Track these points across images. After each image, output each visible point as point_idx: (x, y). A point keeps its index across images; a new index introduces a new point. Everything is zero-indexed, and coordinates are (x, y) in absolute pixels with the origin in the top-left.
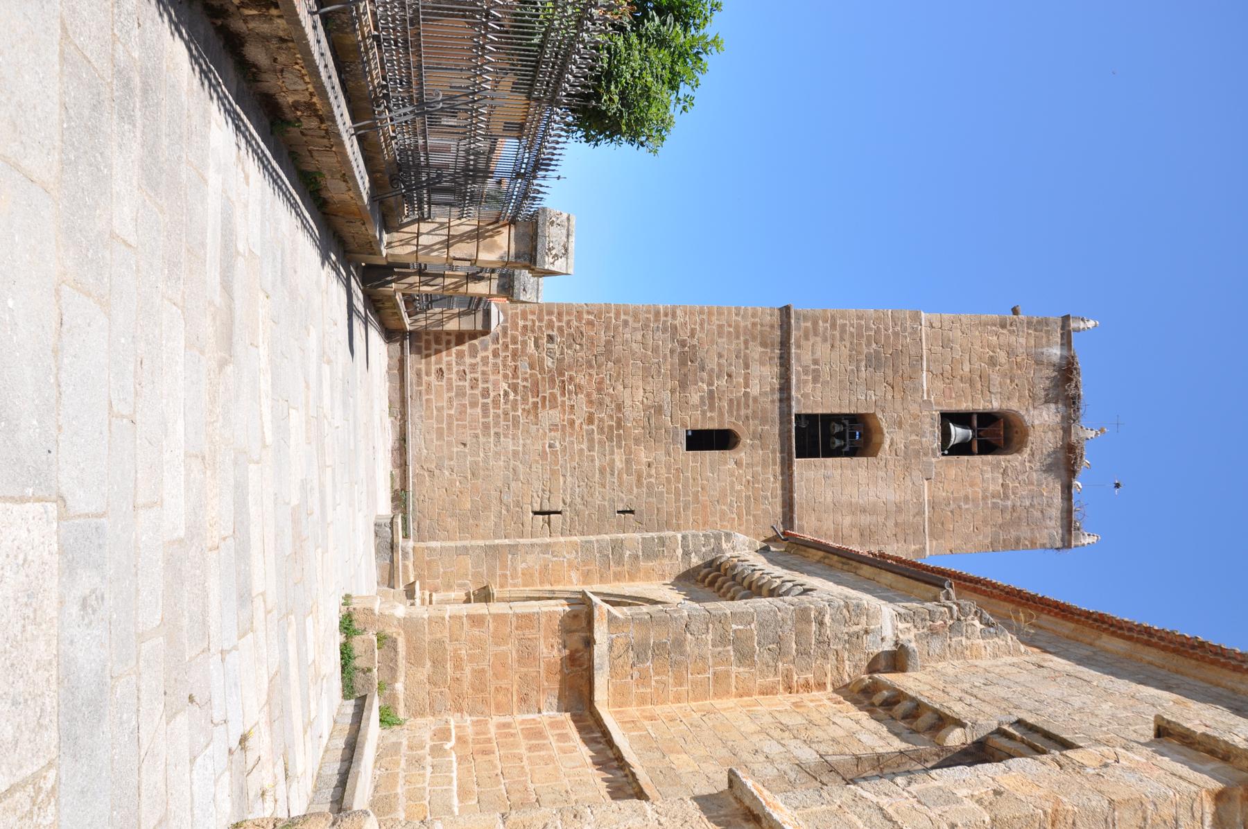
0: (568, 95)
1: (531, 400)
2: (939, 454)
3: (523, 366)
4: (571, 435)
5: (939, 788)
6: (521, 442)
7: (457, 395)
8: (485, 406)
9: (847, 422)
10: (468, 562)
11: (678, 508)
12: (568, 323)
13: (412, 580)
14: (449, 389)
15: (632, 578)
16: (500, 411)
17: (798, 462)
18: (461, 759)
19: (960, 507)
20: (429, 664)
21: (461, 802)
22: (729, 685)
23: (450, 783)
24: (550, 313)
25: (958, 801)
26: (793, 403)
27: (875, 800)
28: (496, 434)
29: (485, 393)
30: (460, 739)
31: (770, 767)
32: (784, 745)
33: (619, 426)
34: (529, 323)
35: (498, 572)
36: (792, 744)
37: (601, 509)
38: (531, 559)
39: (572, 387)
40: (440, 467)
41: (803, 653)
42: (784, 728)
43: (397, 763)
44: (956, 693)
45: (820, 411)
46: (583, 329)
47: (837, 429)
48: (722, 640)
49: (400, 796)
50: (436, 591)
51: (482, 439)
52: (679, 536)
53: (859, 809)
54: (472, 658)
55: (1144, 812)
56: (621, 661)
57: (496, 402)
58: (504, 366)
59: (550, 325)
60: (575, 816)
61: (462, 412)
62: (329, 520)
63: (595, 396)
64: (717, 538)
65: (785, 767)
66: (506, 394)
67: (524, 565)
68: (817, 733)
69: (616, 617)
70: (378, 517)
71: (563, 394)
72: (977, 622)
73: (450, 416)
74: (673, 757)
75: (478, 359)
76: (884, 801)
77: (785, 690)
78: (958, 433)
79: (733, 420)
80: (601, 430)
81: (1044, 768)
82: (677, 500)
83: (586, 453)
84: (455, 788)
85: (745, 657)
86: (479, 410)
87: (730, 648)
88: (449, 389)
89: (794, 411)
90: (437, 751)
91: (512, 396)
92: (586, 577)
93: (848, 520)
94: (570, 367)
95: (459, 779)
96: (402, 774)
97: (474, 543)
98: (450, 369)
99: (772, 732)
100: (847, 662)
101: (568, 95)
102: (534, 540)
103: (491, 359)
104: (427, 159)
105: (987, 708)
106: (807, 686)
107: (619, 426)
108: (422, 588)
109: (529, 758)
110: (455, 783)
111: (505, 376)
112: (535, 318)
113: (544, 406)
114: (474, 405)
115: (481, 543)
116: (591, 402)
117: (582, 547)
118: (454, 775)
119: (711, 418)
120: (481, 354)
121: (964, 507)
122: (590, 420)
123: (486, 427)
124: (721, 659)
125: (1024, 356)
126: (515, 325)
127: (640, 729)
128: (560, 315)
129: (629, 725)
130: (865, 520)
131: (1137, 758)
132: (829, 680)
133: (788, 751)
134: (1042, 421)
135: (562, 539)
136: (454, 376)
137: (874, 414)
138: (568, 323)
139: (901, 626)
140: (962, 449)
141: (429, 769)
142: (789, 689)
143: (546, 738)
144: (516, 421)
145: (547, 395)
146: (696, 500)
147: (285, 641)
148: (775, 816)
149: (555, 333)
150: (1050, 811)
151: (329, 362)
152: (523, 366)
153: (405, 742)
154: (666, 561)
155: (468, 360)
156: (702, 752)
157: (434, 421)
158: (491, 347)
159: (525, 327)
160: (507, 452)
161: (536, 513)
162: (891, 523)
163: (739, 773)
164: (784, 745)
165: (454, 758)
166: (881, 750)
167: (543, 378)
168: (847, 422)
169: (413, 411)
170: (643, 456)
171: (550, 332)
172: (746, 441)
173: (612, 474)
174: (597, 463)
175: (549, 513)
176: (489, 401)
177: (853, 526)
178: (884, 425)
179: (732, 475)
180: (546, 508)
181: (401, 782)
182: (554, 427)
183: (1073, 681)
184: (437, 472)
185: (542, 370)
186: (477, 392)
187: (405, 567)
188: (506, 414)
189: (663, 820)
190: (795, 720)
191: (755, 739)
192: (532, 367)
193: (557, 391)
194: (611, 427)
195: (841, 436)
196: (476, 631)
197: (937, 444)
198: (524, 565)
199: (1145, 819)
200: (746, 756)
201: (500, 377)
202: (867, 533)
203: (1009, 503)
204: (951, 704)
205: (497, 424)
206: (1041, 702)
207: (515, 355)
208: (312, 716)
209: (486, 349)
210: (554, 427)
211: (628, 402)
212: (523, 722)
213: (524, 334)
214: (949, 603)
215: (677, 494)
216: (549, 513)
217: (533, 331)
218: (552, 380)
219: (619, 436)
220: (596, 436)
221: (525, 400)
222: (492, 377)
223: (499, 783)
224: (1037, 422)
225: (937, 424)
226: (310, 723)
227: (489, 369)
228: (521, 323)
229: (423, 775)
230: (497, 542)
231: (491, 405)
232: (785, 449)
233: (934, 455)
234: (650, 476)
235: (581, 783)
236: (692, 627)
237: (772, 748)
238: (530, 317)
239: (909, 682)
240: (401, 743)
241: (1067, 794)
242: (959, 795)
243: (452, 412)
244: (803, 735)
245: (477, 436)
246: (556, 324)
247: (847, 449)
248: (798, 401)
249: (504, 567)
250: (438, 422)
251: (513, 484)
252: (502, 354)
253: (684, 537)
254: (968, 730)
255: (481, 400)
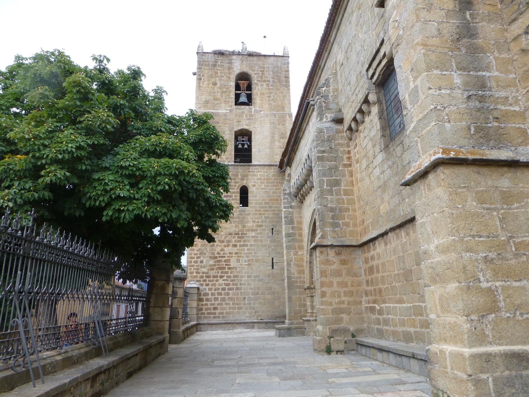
0: (95, 255)
1: (227, 270)
2: (251, 107)
3: (212, 273)
4: (241, 253)
5: (409, 95)
6: (244, 274)
7: (224, 301)
8: (229, 289)
9: (238, 143)
10: (294, 297)
11: (271, 211)
12: (195, 254)
13: (302, 321)
14: (222, 304)
15: (301, 229)
16: (231, 283)
17: (254, 162)
18: (384, 302)
19: (272, 99)
20: (342, 315)
21: (405, 303)
22: (349, 190)
23: (396, 307)
24: (191, 262)
25: (416, 87)
26: (230, 164)
27: (415, 123)
28: (241, 284)
29: (224, 289)
30: (375, 302)
31: (386, 172)
32: (376, 167)
33: (238, 234)
34: (195, 271)
35: (299, 284)
36: (376, 163)
37: (271, 241)
38: (293, 271)
39: (222, 253)
40: (254, 308)
41: (335, 159)
42: (368, 166)
43: (387, 330)
44: (354, 97)
45: (233, 153)
46: (198, 248)
47: (240, 146)
48: (331, 192)
49: (403, 330)
50: (307, 310)
51: (243, 291)
52: (284, 210)
53: (420, 129)
54: (339, 296)
55: (421, 8)
56: (339, 234)
57: (227, 285)
58: (212, 281)
59: (196, 262)
60: (425, 254)
61: (231, 299)
62: (282, 361)
63: (225, 244)
64: (285, 194)
65: (386, 166)
66: (224, 280)
67: (296, 273)
68: (371, 153)
69: (321, 236)
70: (276, 335)
71: (225, 257)
72: (324, 89)
73: (233, 304)
74: (382, 212)
75: (210, 292)
76: (415, 119)
77: (350, 167)
78: (243, 99)
79: (236, 188)
80: (240, 241)
81: (399, 52)
82: (268, 211)
83: (249, 247)
84: (398, 305)
85: (337, 183)
86: (231, 292)
87: (334, 188)
88: (222, 304)
89: (233, 163)
90: (380, 312)
91: (225, 278)
92: (301, 248)
93: (277, 143)
94: (213, 254)
95: (394, 303)
96: (392, 328)
97: (286, 294)
98: (213, 304)
99: (370, 172)
100: (340, 141)
101: (95, 255)
102: (286, 270)
103: (210, 287)
104: (123, 319)
105: (361, 84)
106: (349, 158)
107: (238, 234)
108: (305, 316)
109: (383, 273)
110: (396, 305)
111: (217, 281)
112: (192, 268)
113: (229, 265)
114: (228, 294)
115: (286, 291)
116: (228, 246)
117: (288, 249)
118: (392, 305)
119: (235, 196)
120: (207, 291)
121: (272, 97)
122: (235, 246)
123: (237, 289)
124: (338, 193)
125: (213, 71)
126: (196, 277)
127: (368, 226)
128: (191, 258)
129: (367, 231)
130: (277, 137)
131: (395, 13)
132: (347, 149)
133: (378, 165)
134: (238, 67)
135: (285, 258)
136: (216, 302)
137: (235, 132)
138: (195, 254)
139: (324, 120)
140: (249, 97)
141: (389, 316)
142: (350, 165)
143: (373, 266)
144: (235, 276)
145: (225, 263)
146: (268, 203)
147: (341, 384)
148: (426, 165)
149: (199, 260)
150: (422, 47)
151: (213, 361)
152: (212, 273)
153: (376, 326)
154: (294, 216)
155: (210, 297)
156: (379, 201)
157: (235, 311)
158: (204, 287)
159: (197, 273)
160: (248, 280)
161: (273, 268)
162: (278, 127)
163: (403, 181)
164: (376, 167)
165: (384, 305)
166: (379, 127)
167: (218, 265)
168: (238, 143)
169: (231, 319)
170: (250, 224)
171: (199, 262)
172: (244, 183)
173: (257, 237)
174: (253, 243)
175: (273, 263)
176: (227, 287)
177: (279, 142)
178: (240, 128)
179: (258, 188)
180: (271, 264)
181: (396, 329)
182: (238, 261)
183: (349, 51)
184: (256, 310)
185: (214, 265)
186: (223, 292)
187: (297, 324)
188: (232, 281)
189: (427, 214)
190: (364, 163)
191: (373, 179)
192: (213, 269)
193: (223, 259)
194: (238, 237)
195: (243, 145)
196: (328, 295)
197: (247, 107)
198: (296, 273)
199: (424, 8)
200: (381, 182)
201: (217, 283)
202: (282, 136)
203: (271, 80)
204: (359, 99)
205: (236, 284)
206: (358, 63)
207: (208, 277)
208: (370, 369)
209: (205, 289)
210: (238, 261)
211: (228, 231)
212: (365, 275)
213: (199, 273)
214: (316, 100)
215: (266, 211)
216: (273, 263)
217: (198, 269)
218: (219, 261)
219: (242, 234)
220: (242, 243)
221: (227, 273)
222: (217, 287)
223: (395, 286)
224: (239, 68)
225: (239, 107)
226: (374, 371)
227: (213, 287)
228: (195, 274)
229: (392, 319)
230: (286, 285)
231: (229, 287)
232: (250, 166)
233: (252, 108)
234: (258, 222)
235: (395, 250)
236: (325, 204)
237: (377, 172)
238: (192, 271)
239: (348, 115)
240: (377, 328)
241: (413, 40)
242: (413, 87)
243: (231, 303)
244: (371, 159)
245: (241, 293)
246: (195, 259)
247: (248, 143)
248: (229, 162)
249: (297, 282)
250: (235, 309)
251: (261, 278)
252: (207, 282)
253: (285, 208)
254: (370, 92)
255: (227, 291)
